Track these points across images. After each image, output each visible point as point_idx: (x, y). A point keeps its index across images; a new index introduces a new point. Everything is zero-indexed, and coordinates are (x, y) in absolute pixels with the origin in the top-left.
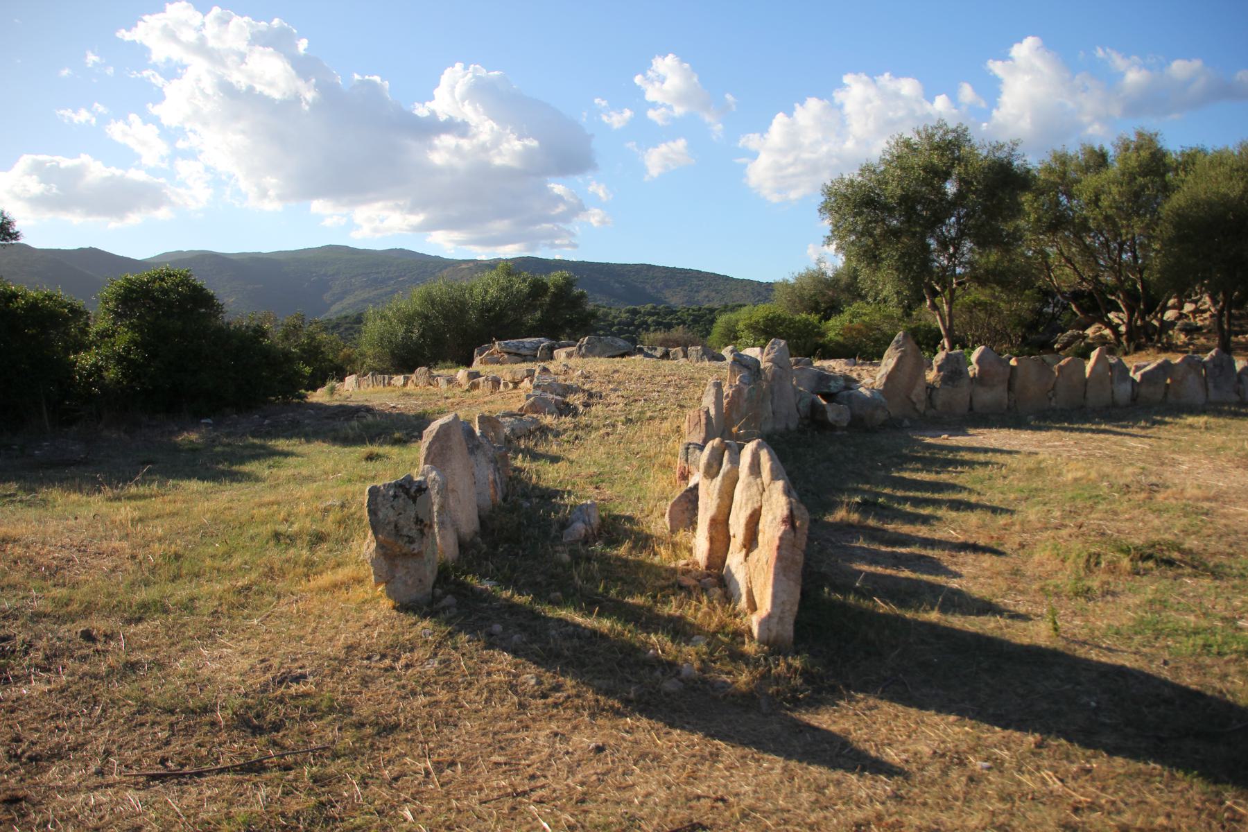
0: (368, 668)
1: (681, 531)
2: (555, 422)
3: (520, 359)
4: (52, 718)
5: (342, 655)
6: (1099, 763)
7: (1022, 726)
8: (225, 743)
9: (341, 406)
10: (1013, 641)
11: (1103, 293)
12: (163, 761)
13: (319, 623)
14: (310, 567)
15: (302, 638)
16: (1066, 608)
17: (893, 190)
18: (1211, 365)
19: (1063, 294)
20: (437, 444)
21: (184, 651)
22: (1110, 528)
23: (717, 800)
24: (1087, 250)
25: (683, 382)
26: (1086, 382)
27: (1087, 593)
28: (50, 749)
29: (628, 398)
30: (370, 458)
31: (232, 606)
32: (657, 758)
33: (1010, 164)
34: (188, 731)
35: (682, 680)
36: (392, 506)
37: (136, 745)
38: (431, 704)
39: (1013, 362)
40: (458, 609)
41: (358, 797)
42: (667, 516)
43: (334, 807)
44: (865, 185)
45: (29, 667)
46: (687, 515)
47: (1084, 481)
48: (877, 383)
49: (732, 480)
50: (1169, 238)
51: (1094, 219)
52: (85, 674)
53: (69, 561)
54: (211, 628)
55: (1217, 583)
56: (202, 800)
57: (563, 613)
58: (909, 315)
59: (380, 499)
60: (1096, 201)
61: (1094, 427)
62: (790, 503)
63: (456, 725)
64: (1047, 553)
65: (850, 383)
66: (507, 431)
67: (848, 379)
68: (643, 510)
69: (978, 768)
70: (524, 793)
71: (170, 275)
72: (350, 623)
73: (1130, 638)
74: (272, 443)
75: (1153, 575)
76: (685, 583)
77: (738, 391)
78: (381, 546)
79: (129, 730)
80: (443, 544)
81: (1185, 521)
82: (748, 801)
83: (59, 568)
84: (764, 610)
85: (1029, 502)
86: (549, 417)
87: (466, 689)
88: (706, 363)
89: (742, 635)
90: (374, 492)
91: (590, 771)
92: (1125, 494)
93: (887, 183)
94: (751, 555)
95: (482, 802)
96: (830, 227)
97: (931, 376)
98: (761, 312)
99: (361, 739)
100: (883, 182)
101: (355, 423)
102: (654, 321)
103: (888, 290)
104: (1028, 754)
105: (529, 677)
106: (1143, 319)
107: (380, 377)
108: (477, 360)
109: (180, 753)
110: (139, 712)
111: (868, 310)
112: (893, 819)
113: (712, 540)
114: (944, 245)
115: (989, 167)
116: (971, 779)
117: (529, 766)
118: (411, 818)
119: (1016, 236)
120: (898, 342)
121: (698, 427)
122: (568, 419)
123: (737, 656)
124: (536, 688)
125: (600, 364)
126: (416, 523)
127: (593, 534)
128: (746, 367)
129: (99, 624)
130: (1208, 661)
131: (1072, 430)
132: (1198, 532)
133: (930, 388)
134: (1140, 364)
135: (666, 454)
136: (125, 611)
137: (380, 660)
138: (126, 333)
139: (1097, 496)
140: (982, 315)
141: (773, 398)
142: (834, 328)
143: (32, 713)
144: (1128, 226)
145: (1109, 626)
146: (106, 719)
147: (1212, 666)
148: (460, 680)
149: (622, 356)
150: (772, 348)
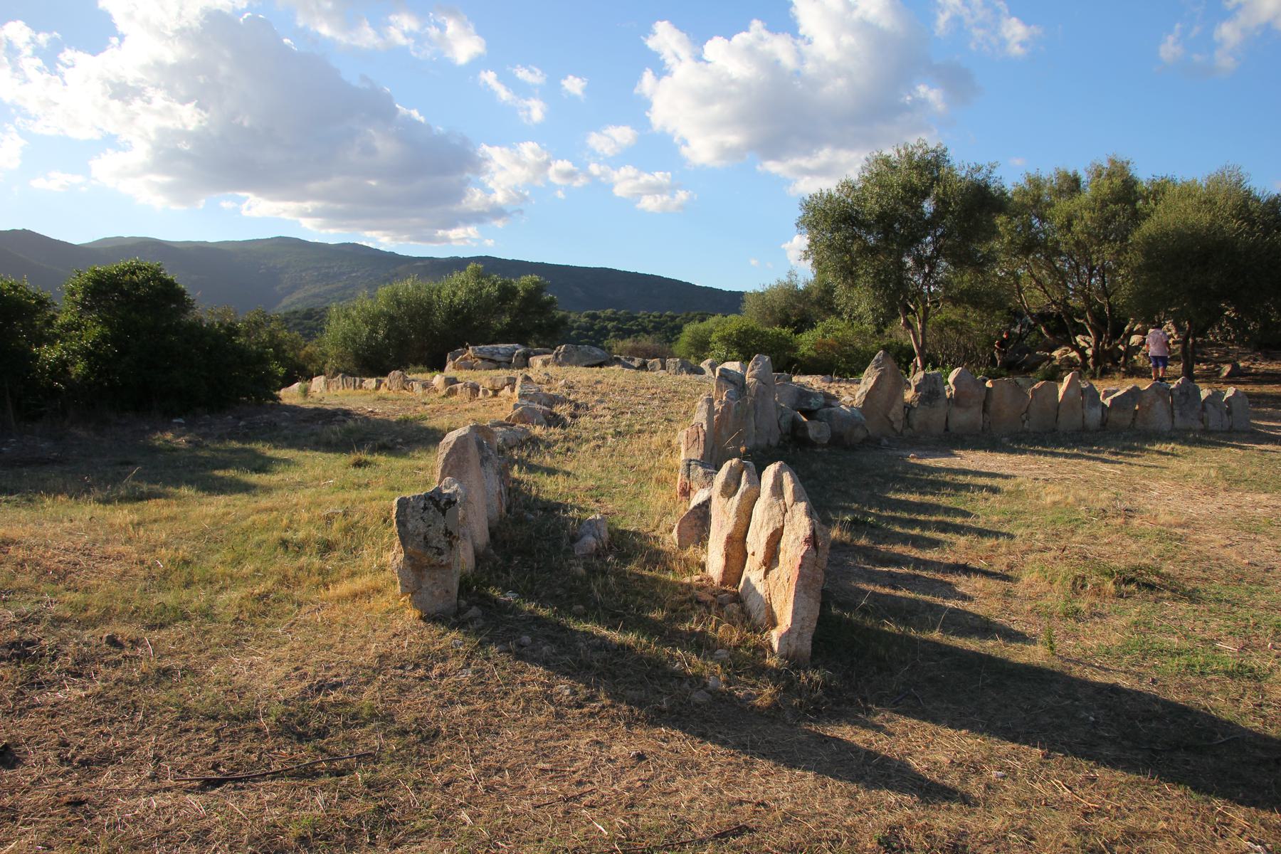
0: (402, 676)
1: (691, 547)
2: (544, 433)
3: (495, 365)
4: (94, 722)
5: (375, 664)
6: (1102, 773)
7: (1029, 739)
8: (273, 749)
9: (316, 409)
10: (1012, 659)
11: (1070, 317)
12: (216, 766)
13: (345, 632)
14: (325, 579)
15: (331, 646)
16: (1061, 627)
17: (872, 206)
18: (1177, 393)
19: (1031, 315)
20: (455, 456)
21: (213, 658)
22: (1092, 551)
23: (758, 804)
24: (1055, 271)
25: (667, 395)
26: (1058, 406)
27: (1076, 614)
28: (100, 753)
29: (615, 410)
30: (358, 464)
31: (253, 614)
32: (697, 765)
33: (987, 186)
34: (235, 738)
35: (709, 692)
36: (422, 518)
37: (185, 751)
38: (470, 713)
39: (989, 384)
40: (484, 620)
41: (414, 801)
42: (675, 531)
43: (393, 811)
44: (844, 201)
45: (59, 672)
46: (696, 531)
47: (1063, 505)
48: (856, 401)
49: (751, 500)
50: (1139, 266)
51: (1066, 244)
52: (120, 680)
53: (76, 565)
54: (236, 635)
55: (1195, 606)
56: (262, 804)
57: (582, 626)
58: (880, 331)
59: (409, 510)
60: (1068, 225)
61: (1066, 451)
62: (813, 524)
63: (498, 734)
64: (1035, 574)
65: (830, 399)
66: (499, 440)
67: (827, 396)
68: (648, 526)
69: (993, 776)
70: (575, 798)
71: (140, 269)
72: (377, 633)
73: (1119, 658)
74: (260, 447)
75: (1135, 598)
76: (702, 599)
77: (727, 406)
78: (409, 557)
79: (175, 735)
80: (464, 558)
81: (1160, 546)
82: (787, 806)
83: (67, 573)
84: (784, 625)
85: (1012, 524)
86: (538, 428)
87: (502, 698)
88: (685, 376)
89: (762, 650)
90: (403, 503)
91: (634, 777)
92: (1102, 519)
93: (865, 200)
94: (771, 572)
95: (536, 807)
96: (808, 242)
97: (909, 395)
98: (734, 323)
99: (406, 746)
100: (861, 200)
101: (336, 428)
102: (613, 327)
103: (864, 307)
104: (1038, 764)
105: (563, 688)
106: (1109, 344)
107: (350, 379)
108: (450, 365)
109: (232, 759)
110: (181, 718)
111: (841, 325)
112: (923, 822)
113: (728, 557)
114: (920, 262)
115: (967, 188)
116: (988, 787)
117: (574, 772)
118: (469, 821)
119: (990, 259)
120: (878, 361)
121: (696, 443)
122: (558, 430)
123: (760, 671)
124: (571, 698)
125: (581, 374)
126: (445, 535)
127: (604, 547)
128: (732, 382)
129: (125, 631)
130: (1193, 680)
131: (1046, 454)
132: (1173, 557)
133: (908, 407)
134: (1111, 388)
135: (660, 468)
136: (145, 618)
137: (413, 669)
138: (94, 327)
139: (1076, 520)
140: (953, 334)
141: (756, 413)
142: (807, 342)
143: (73, 718)
144: (1099, 252)
145: (1099, 646)
146: (149, 725)
147: (1197, 685)
148: (495, 690)
149: (601, 365)
150: (756, 364)
